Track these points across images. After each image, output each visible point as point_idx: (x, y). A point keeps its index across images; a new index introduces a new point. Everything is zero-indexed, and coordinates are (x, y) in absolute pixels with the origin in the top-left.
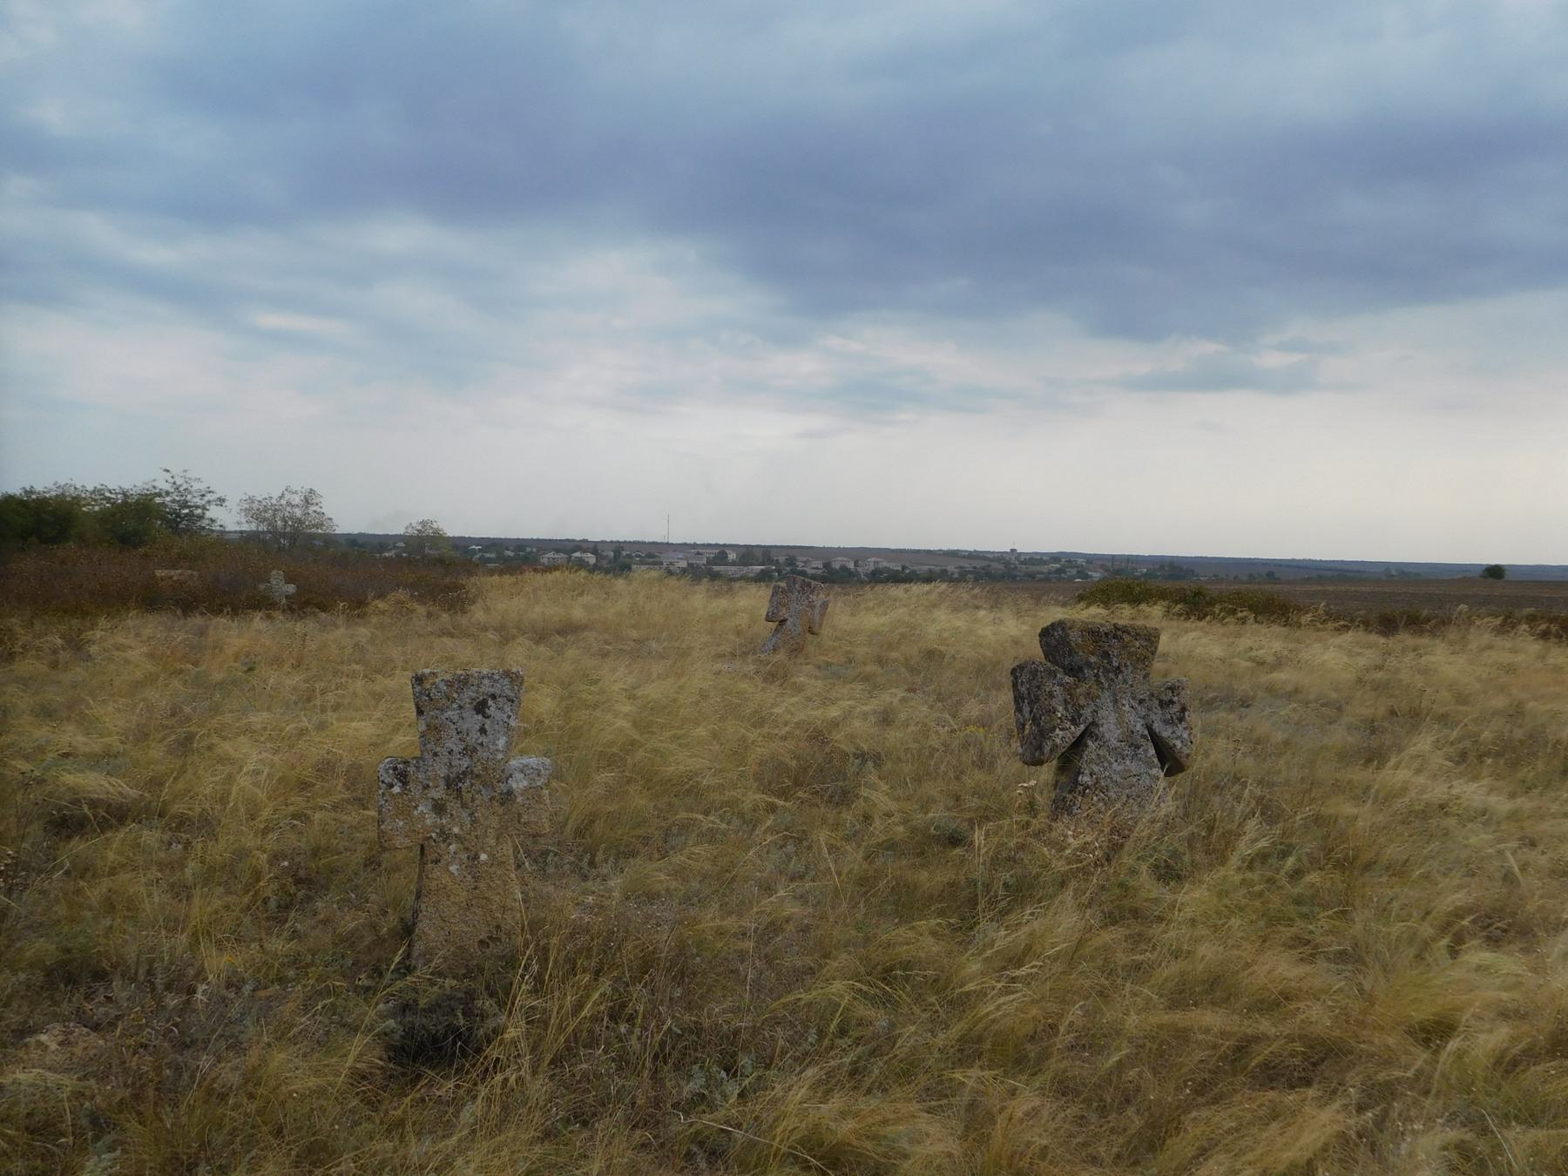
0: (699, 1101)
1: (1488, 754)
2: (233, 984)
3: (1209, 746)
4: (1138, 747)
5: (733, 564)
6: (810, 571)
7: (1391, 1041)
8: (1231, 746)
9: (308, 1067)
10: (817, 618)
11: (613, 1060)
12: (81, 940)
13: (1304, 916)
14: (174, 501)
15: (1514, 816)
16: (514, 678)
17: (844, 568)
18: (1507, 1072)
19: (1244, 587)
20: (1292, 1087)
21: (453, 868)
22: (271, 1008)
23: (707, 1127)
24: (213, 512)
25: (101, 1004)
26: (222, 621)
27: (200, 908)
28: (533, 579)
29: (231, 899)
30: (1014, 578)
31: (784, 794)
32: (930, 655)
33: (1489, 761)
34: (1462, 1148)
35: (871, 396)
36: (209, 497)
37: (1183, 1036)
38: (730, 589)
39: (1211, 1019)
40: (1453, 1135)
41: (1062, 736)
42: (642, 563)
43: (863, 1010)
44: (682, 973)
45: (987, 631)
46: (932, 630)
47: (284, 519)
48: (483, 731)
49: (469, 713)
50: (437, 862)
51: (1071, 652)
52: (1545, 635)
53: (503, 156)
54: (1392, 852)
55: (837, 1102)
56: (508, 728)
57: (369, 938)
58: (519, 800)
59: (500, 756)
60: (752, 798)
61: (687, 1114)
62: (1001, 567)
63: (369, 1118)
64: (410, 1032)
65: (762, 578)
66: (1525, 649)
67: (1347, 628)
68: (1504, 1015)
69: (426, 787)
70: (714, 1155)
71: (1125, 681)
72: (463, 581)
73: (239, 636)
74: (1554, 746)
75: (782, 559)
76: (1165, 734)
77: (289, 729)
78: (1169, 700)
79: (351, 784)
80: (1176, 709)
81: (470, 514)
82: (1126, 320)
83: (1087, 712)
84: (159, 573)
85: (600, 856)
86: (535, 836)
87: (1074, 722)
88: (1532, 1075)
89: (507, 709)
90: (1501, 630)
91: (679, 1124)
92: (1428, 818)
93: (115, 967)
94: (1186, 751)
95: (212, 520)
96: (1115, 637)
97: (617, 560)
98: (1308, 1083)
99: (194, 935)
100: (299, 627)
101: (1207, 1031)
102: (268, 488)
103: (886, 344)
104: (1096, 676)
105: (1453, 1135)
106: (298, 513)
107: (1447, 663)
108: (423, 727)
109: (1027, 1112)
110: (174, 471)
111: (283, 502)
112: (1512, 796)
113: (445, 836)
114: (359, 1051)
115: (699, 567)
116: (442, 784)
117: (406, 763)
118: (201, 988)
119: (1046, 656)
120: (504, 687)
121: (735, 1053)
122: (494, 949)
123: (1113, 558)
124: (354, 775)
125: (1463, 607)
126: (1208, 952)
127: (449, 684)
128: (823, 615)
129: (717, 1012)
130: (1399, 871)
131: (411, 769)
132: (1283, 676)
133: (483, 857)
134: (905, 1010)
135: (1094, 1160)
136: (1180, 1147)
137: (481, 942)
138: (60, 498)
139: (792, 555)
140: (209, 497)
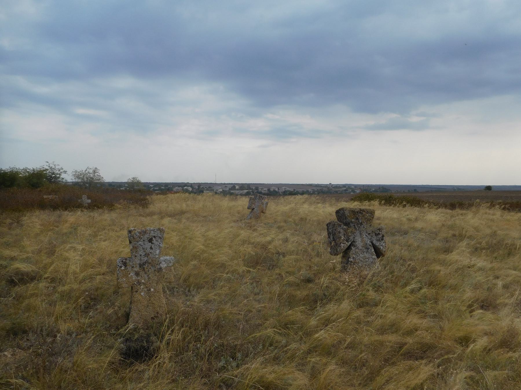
0: (223, 369)
1: (484, 249)
2: (69, 333)
3: (392, 247)
5: (238, 190)
6: (263, 192)
7: (449, 343)
8: (400, 248)
9: (94, 360)
10: (264, 208)
11: (195, 356)
12: (18, 320)
13: (423, 303)
14: (49, 172)
15: (492, 269)
16: (161, 231)
17: (274, 191)
18: (487, 353)
19: (405, 194)
20: (417, 360)
21: (142, 294)
22: (82, 341)
23: (226, 377)
24: (63, 176)
25: (25, 341)
26: (66, 213)
27: (59, 308)
28: (170, 196)
29: (69, 305)
31: (254, 267)
32: (302, 219)
33: (484, 251)
34: (471, 378)
35: (282, 133)
37: (382, 343)
38: (236, 198)
39: (392, 338)
40: (468, 374)
41: (344, 246)
42: (207, 190)
43: (278, 338)
44: (218, 326)
45: (321, 211)
46: (301, 210)
47: (87, 178)
48: (151, 248)
49: (146, 242)
50: (137, 292)
52: (504, 209)
53: (156, 54)
54: (452, 281)
55: (269, 369)
56: (160, 247)
57: (114, 318)
58: (164, 271)
59: (157, 256)
60: (242, 269)
61: (219, 373)
62: (327, 189)
63: (115, 377)
64: (129, 348)
65: (247, 194)
66: (497, 213)
68: (486, 334)
69: (133, 267)
70: (228, 386)
71: (364, 227)
72: (148, 197)
73: (71, 217)
74: (506, 245)
75: (254, 188)
77: (86, 248)
78: (378, 233)
79: (109, 266)
80: (380, 236)
81: (149, 175)
82: (366, 107)
83: (351, 238)
84: (45, 197)
85: (192, 288)
86: (170, 282)
87: (347, 241)
88: (495, 354)
89: (159, 241)
90: (490, 208)
91: (217, 376)
92: (463, 271)
93: (30, 329)
94: (384, 250)
95: (63, 179)
97: (198, 189)
98: (422, 358)
99: (57, 317)
100: (92, 214)
101: (390, 342)
102: (81, 168)
103: (287, 116)
104: (354, 226)
105: (468, 374)
106: (92, 176)
107: (472, 220)
108: (131, 247)
109: (332, 370)
112: (491, 262)
113: (139, 283)
114: (112, 355)
115: (226, 191)
116: (138, 266)
117: (126, 259)
118: (59, 335)
119: (338, 219)
120: (158, 233)
121: (235, 353)
122: (156, 320)
123: (363, 186)
124: (110, 263)
125: (478, 200)
126: (391, 316)
127: (140, 233)
128: (266, 207)
129: (230, 339)
130: (454, 288)
131: (128, 261)
132: (419, 225)
133: (152, 290)
134: (291, 337)
135: (352, 385)
136: (380, 380)
137: (152, 318)
138: (11, 172)
139: (257, 186)
140: (61, 171)
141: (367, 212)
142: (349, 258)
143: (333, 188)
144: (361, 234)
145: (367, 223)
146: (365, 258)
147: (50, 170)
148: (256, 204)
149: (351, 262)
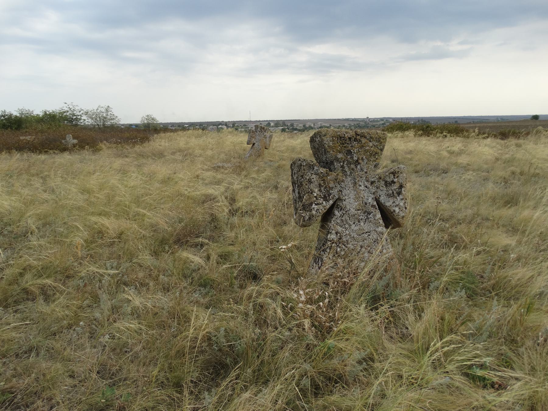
4: (369, 213)
5: (273, 127)
6: (298, 128)
10: (268, 143)
14: (70, 114)
30: (368, 127)
36: (81, 113)
41: (319, 208)
51: (326, 152)
67: (488, 137)
71: (362, 170)
75: (289, 124)
76: (388, 204)
80: (395, 187)
83: (335, 192)
84: (21, 138)
87: (325, 199)
94: (402, 214)
96: (356, 140)
104: (342, 167)
106: (105, 115)
110: (68, 103)
111: (98, 111)
128: (270, 141)
132: (463, 160)
141: (371, 139)
142: (329, 232)
143: (371, 122)
144: (355, 183)
145: (369, 160)
147: (70, 112)
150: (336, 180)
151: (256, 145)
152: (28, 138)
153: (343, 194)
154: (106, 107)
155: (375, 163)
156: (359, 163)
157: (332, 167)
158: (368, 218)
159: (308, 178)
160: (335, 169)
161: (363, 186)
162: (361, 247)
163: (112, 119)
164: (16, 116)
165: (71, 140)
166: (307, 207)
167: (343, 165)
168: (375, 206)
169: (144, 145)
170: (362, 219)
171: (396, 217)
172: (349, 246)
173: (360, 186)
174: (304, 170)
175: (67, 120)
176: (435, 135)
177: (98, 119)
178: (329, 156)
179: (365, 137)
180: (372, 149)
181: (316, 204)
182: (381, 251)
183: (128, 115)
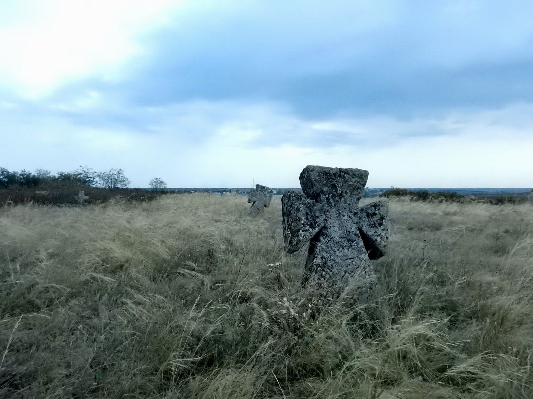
10: (268, 201)
14: (84, 176)
36: (94, 175)
41: (306, 234)
51: (313, 185)
71: (345, 202)
76: (370, 234)
83: (320, 220)
84: (37, 192)
87: (312, 226)
94: (383, 243)
96: (340, 176)
104: (328, 199)
106: (116, 177)
110: (83, 166)
111: (111, 173)
144: (339, 214)
146: (345, 258)
148: (258, 196)
149: (318, 265)
150: (322, 210)
151: (256, 203)
152: (44, 193)
153: (328, 222)
154: (118, 170)
155: (357, 197)
156: (343, 196)
157: (318, 199)
158: (352, 246)
159: (296, 207)
160: (321, 201)
161: (346, 216)
162: (345, 272)
163: (122, 181)
164: (34, 176)
165: (82, 196)
166: (295, 233)
167: (328, 197)
168: (358, 234)
169: (152, 202)
170: (345, 246)
171: (378, 247)
172: (333, 270)
173: (344, 216)
174: (293, 200)
175: (81, 182)
176: (431, 201)
177: (110, 181)
178: (315, 189)
179: (349, 174)
180: (355, 184)
181: (303, 231)
182: (362, 273)
183: (139, 180)
